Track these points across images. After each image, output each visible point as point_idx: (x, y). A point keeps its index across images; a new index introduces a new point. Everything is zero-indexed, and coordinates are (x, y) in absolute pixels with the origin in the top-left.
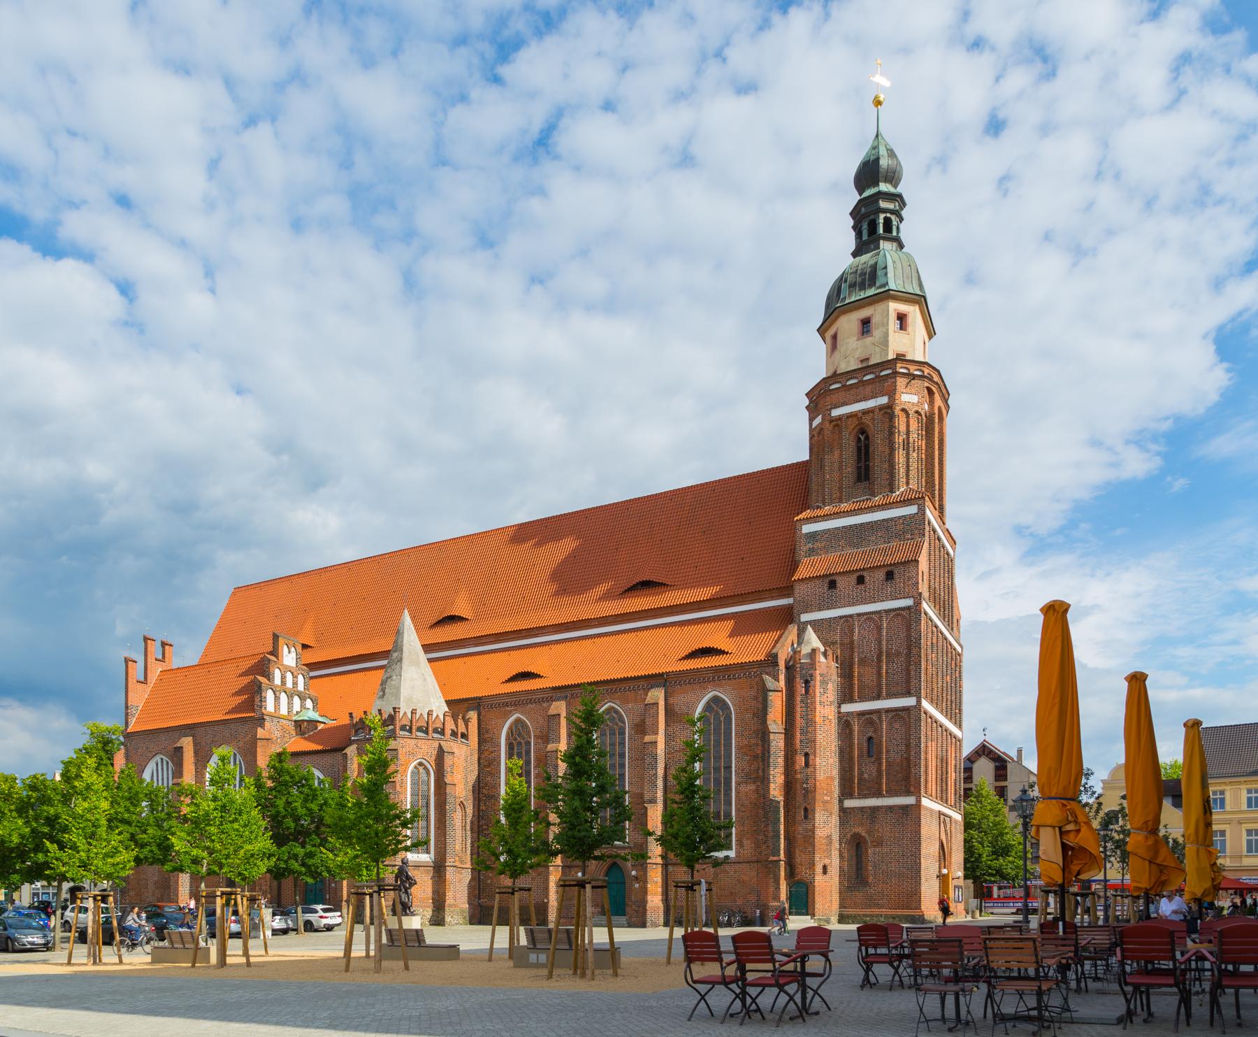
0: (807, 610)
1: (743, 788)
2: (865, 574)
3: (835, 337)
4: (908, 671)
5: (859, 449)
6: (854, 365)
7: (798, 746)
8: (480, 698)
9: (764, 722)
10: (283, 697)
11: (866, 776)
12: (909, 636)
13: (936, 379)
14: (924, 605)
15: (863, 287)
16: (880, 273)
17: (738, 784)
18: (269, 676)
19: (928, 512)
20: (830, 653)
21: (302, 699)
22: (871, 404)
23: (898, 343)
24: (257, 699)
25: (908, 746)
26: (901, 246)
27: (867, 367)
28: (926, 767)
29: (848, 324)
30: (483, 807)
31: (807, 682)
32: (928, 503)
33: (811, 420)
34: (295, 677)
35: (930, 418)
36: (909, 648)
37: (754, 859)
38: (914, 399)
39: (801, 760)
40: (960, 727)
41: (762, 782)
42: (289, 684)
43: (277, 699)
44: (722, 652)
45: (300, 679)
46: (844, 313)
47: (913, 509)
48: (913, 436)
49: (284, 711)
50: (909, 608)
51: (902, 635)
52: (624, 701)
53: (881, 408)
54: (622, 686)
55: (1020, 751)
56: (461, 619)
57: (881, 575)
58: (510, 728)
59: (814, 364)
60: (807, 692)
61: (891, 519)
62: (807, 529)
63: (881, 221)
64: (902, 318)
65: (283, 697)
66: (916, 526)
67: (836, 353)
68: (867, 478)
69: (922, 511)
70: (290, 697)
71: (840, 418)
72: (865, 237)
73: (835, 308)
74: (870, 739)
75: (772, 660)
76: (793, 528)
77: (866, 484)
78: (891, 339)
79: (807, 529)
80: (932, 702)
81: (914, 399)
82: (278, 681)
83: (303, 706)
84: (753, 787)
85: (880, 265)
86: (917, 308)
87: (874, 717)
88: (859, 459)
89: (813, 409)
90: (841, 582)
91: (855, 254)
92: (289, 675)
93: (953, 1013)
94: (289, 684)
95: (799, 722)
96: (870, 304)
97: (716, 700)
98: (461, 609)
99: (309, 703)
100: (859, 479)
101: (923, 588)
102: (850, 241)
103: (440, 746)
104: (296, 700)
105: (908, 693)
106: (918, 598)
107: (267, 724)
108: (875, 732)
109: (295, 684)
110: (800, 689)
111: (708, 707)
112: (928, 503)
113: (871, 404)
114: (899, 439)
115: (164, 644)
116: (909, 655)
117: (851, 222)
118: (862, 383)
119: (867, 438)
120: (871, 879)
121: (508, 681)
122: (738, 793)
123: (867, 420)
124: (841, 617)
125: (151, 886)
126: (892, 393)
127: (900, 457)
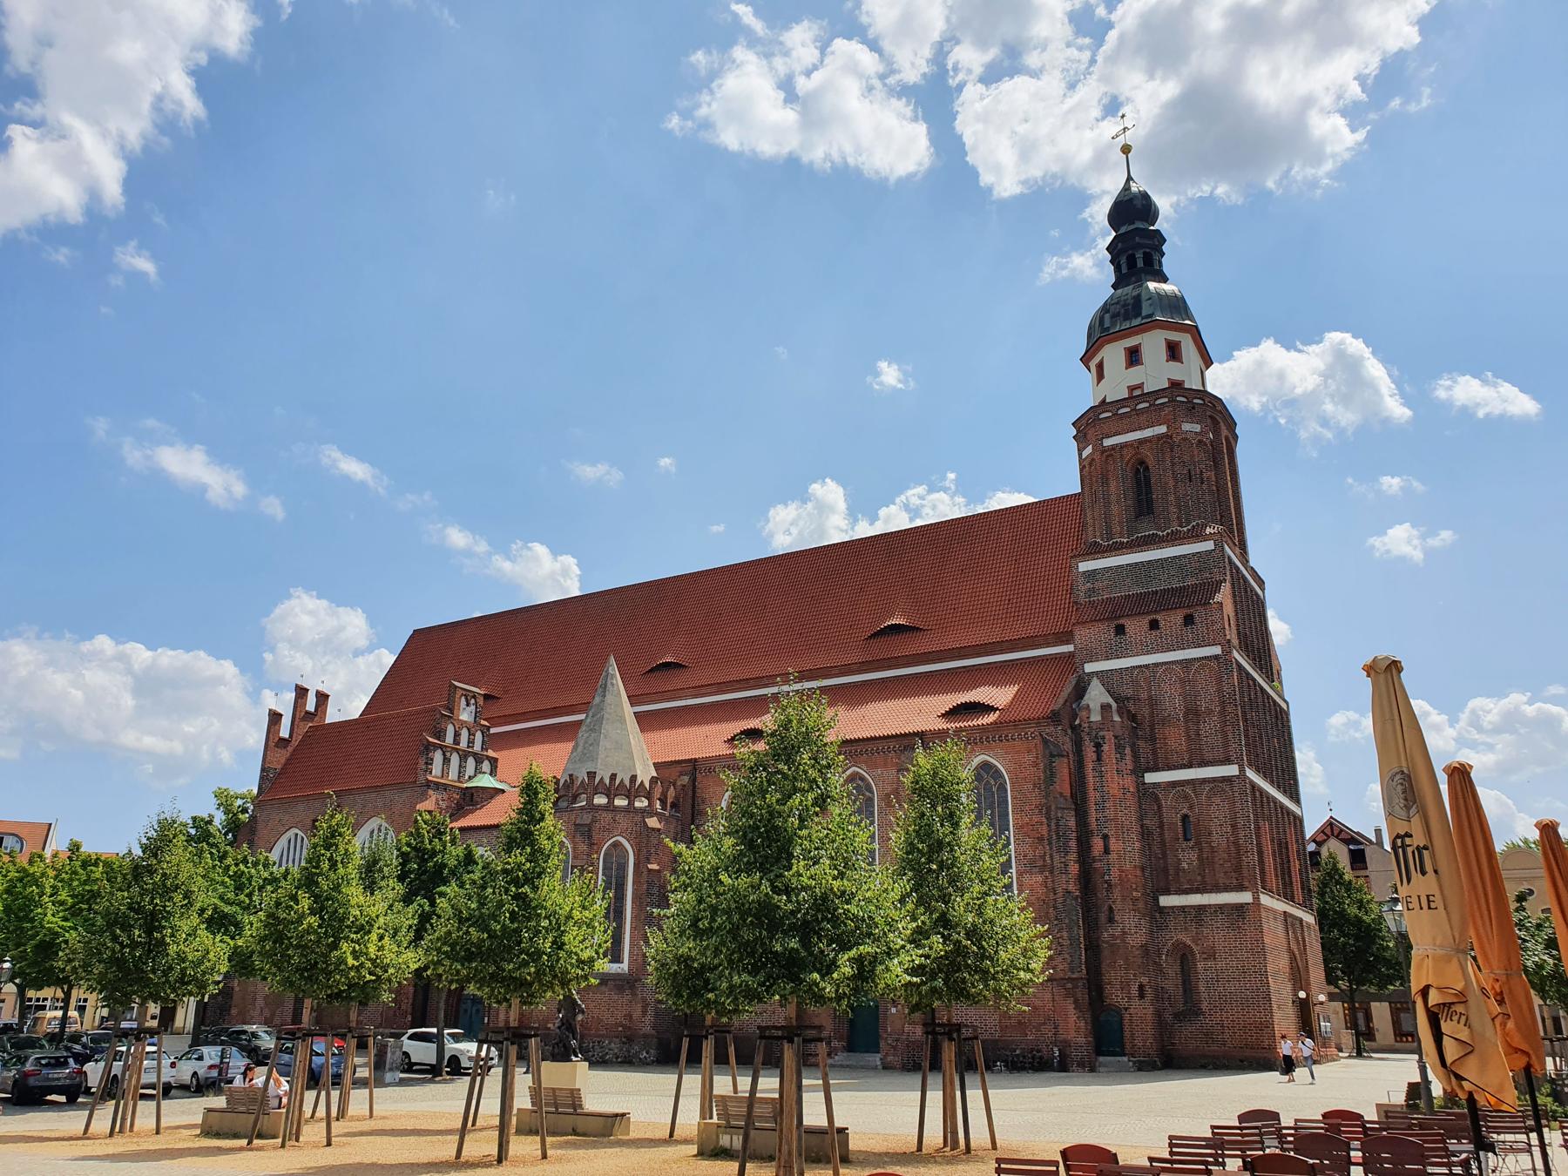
1: (1026, 878)
2: (1158, 617)
3: (1100, 366)
5: (1138, 482)
7: (1094, 826)
10: (455, 759)
15: (1127, 318)
18: (440, 734)
22: (1148, 433)
29: (1113, 355)
31: (1098, 746)
33: (1080, 451)
38: (1197, 428)
39: (1097, 844)
42: (463, 744)
43: (446, 761)
46: (1109, 342)
50: (1216, 657)
52: (872, 766)
53: (1159, 437)
57: (1178, 617)
59: (1083, 394)
60: (1099, 759)
61: (1184, 556)
62: (1084, 566)
68: (1150, 511)
71: (1113, 447)
72: (1124, 270)
73: (1103, 331)
74: (1185, 818)
79: (1084, 566)
80: (1258, 771)
82: (449, 740)
84: (1040, 879)
89: (1081, 438)
91: (1115, 286)
94: (463, 744)
95: (1093, 796)
96: (1137, 333)
97: (985, 766)
99: (486, 766)
102: (1109, 274)
108: (1191, 808)
109: (471, 742)
110: (1089, 753)
113: (1148, 433)
119: (1147, 468)
120: (1204, 1006)
124: (1134, 668)
125: (260, 1002)
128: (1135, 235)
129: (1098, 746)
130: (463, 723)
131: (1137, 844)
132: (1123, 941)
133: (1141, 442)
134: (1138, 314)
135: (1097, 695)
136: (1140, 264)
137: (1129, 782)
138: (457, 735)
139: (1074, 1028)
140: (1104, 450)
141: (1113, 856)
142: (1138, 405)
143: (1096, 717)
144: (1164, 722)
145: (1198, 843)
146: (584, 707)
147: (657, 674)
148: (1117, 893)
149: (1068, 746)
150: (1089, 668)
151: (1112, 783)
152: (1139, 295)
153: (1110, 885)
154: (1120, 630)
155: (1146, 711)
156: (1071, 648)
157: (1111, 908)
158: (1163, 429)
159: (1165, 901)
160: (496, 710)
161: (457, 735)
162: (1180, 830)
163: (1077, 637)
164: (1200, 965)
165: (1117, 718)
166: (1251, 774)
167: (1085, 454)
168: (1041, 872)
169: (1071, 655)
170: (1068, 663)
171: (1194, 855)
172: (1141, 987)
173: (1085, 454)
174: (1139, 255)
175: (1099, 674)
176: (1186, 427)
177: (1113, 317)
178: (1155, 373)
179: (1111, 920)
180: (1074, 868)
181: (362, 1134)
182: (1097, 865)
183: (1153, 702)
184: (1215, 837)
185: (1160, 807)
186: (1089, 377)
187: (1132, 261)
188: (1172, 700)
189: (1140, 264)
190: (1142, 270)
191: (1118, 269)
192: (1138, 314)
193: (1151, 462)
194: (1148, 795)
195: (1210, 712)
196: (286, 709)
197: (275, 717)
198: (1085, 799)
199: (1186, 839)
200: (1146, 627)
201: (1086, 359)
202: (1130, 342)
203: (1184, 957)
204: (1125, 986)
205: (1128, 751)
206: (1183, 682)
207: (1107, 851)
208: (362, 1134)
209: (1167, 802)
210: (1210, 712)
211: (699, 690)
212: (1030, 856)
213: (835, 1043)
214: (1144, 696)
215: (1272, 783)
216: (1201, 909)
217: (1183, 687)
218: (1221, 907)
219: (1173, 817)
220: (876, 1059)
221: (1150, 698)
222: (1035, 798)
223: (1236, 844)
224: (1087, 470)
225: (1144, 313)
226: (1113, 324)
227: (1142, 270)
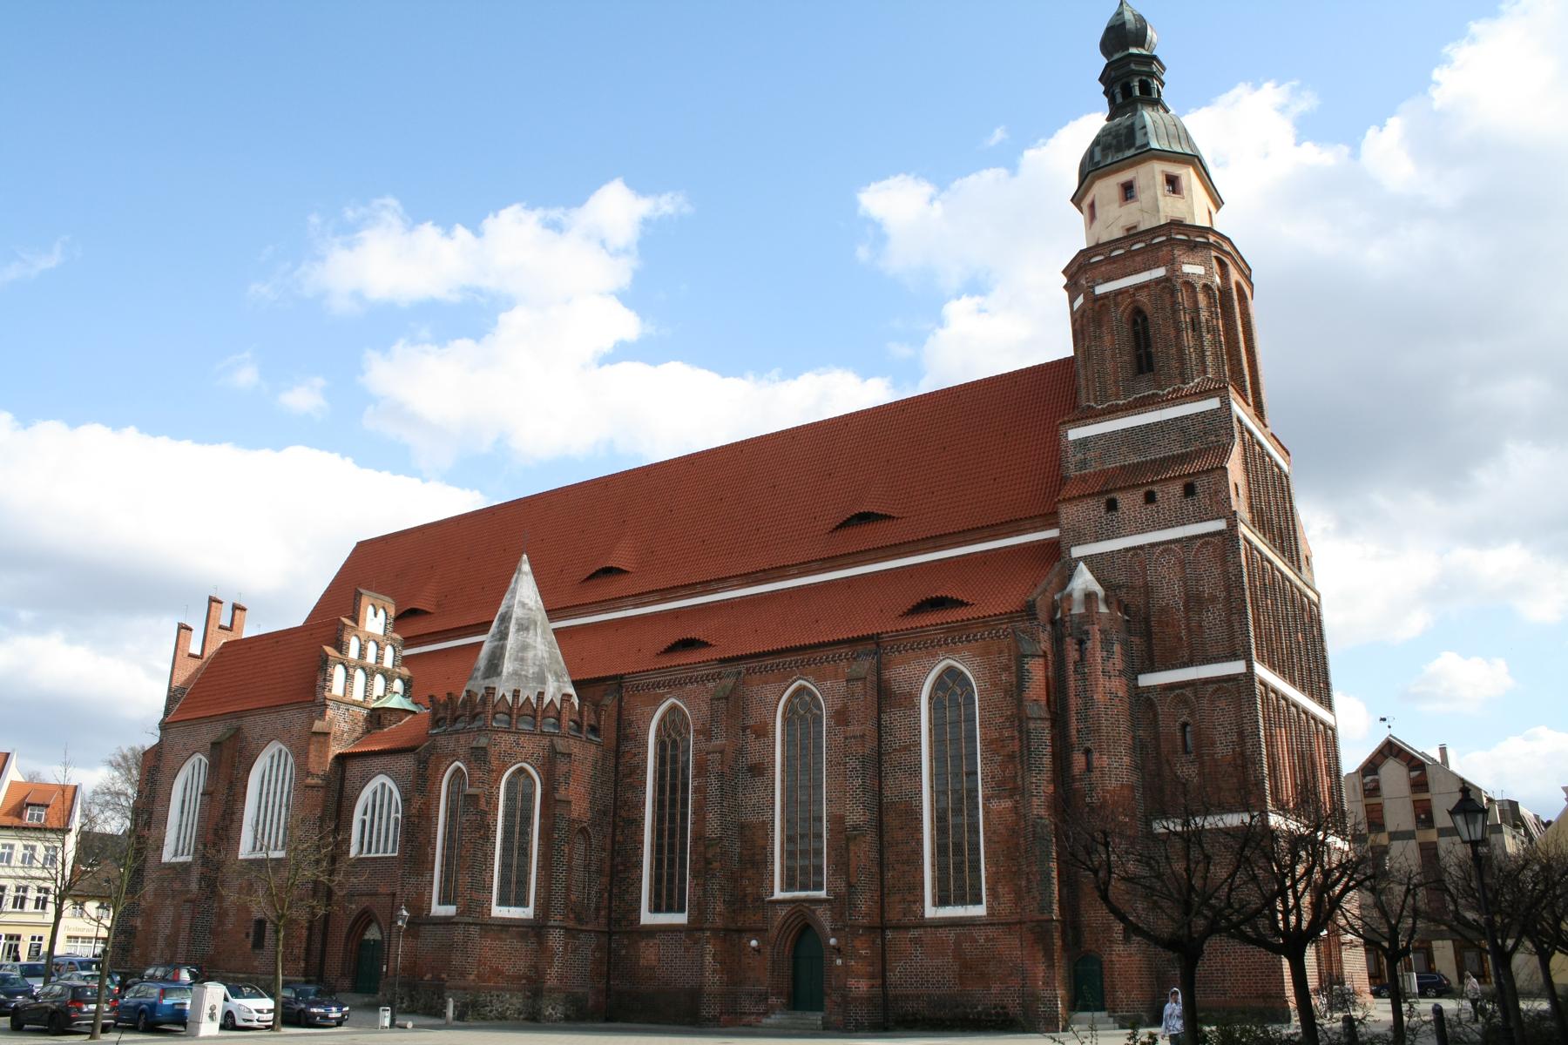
0: (1081, 540)
1: (995, 805)
2: (1155, 488)
3: (1092, 206)
4: (1231, 626)
5: (1136, 334)
6: (1118, 233)
7: (1074, 739)
8: (622, 676)
9: (1020, 702)
12: (1225, 572)
13: (1227, 248)
14: (1243, 530)
15: (1119, 149)
16: (1139, 134)
17: (987, 799)
18: (340, 646)
19: (1235, 407)
20: (1113, 600)
21: (389, 678)
23: (1170, 208)
24: (320, 678)
26: (1167, 111)
27: (1132, 234)
28: (1273, 767)
29: (1108, 188)
30: (619, 838)
31: (1081, 642)
32: (1233, 394)
33: (1072, 302)
35: (1225, 292)
36: (1228, 588)
38: (1200, 270)
39: (1079, 760)
40: (1330, 707)
41: (1022, 795)
42: (371, 658)
43: (349, 677)
44: (961, 604)
45: (389, 652)
46: (1100, 177)
47: (1214, 403)
48: (1204, 315)
49: (358, 695)
50: (1220, 533)
51: (1217, 572)
52: (820, 679)
53: (1158, 281)
54: (819, 655)
55: (1443, 750)
56: (619, 571)
57: (1177, 489)
58: (663, 719)
59: (1073, 236)
61: (1187, 417)
62: (1075, 434)
64: (1173, 182)
65: (359, 676)
66: (1218, 429)
67: (1096, 223)
68: (1150, 368)
69: (1226, 405)
71: (1106, 296)
72: (1119, 99)
73: (1091, 169)
74: (1185, 725)
75: (1029, 611)
76: (1056, 438)
77: (1150, 375)
78: (1161, 204)
79: (1075, 434)
80: (1272, 667)
81: (1200, 270)
82: (353, 653)
84: (1008, 803)
85: (1138, 125)
86: (1191, 170)
87: (1188, 692)
88: (1138, 346)
89: (1072, 287)
90: (1124, 500)
91: (1109, 119)
94: (371, 658)
95: (1074, 703)
96: (1131, 166)
97: (950, 671)
98: (620, 558)
101: (1240, 505)
103: (553, 746)
104: (379, 681)
105: (1233, 657)
106: (1232, 519)
107: (330, 713)
108: (1191, 714)
109: (379, 658)
111: (939, 684)
112: (1233, 394)
114: (1185, 318)
115: (236, 608)
116: (1228, 599)
117: (1102, 88)
118: (1131, 254)
119: (1145, 319)
121: (671, 649)
122: (986, 813)
123: (1143, 297)
124: (1127, 550)
125: (161, 943)
126: (1171, 263)
127: (1188, 339)
129: (1081, 642)
131: (1126, 760)
133: (1139, 288)
134: (1131, 145)
135: (1084, 580)
137: (1117, 685)
141: (1096, 774)
143: (1078, 609)
145: (1199, 756)
147: (594, 582)
151: (1106, 684)
154: (1112, 506)
155: (1140, 601)
156: (1053, 533)
158: (1160, 272)
160: (418, 626)
161: (362, 651)
162: (1179, 742)
163: (1063, 516)
165: (1103, 609)
166: (1261, 671)
168: (1011, 796)
170: (1053, 553)
182: (1077, 785)
183: (1148, 590)
185: (1156, 715)
186: (1078, 218)
187: (1127, 90)
188: (1170, 591)
191: (1112, 101)
192: (1131, 145)
193: (1148, 309)
194: (1144, 702)
195: (1213, 599)
198: (1065, 708)
199: (1186, 752)
201: (1077, 200)
202: (1125, 176)
205: (1117, 648)
206: (1182, 564)
207: (1089, 767)
211: (640, 598)
213: (773, 1000)
215: (1293, 683)
217: (1183, 568)
219: (1169, 724)
220: (816, 1018)
221: (1146, 584)
223: (1242, 754)
224: (1085, 324)
225: (1138, 143)
226: (1105, 156)
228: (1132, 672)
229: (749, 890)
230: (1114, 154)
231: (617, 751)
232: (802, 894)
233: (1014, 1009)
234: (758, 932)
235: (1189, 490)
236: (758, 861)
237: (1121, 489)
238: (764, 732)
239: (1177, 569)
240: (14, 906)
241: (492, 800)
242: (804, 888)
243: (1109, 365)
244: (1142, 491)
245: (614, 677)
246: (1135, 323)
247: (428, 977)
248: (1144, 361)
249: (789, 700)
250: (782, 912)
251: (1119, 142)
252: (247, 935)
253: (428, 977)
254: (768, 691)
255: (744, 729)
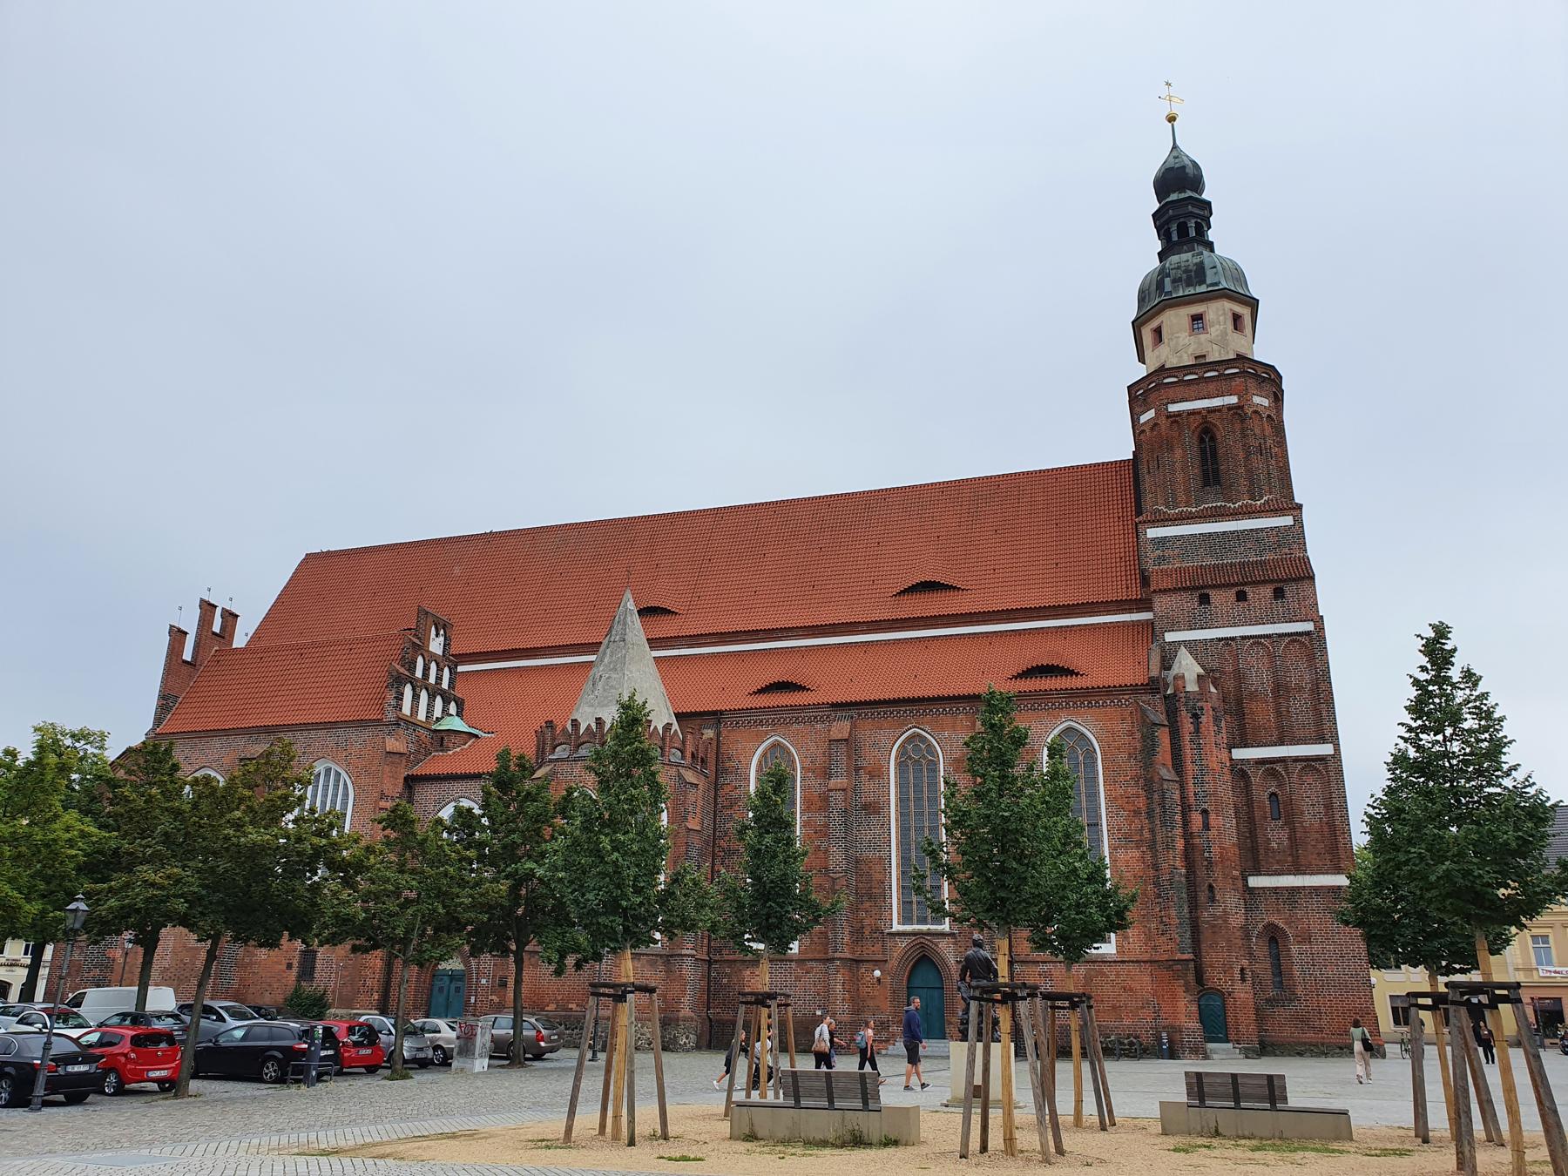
1: (1121, 854)
2: (1247, 589)
5: (1203, 451)
8: (721, 712)
10: (424, 695)
11: (1274, 845)
25: (1329, 807)
27: (1201, 364)
29: (1175, 320)
31: (1196, 716)
34: (440, 670)
37: (1146, 957)
39: (1197, 819)
42: (432, 680)
43: (416, 697)
46: (1171, 306)
49: (422, 716)
50: (1308, 633)
53: (1230, 408)
57: (1267, 591)
60: (1197, 730)
61: (1262, 530)
62: (1153, 533)
63: (1174, 227)
65: (424, 695)
68: (1217, 481)
70: (432, 698)
71: (1179, 414)
72: (1175, 237)
79: (1153, 533)
83: (445, 711)
87: (1278, 768)
88: (1204, 461)
90: (1216, 597)
91: (1162, 256)
92: (433, 666)
93: (992, 1113)
94: (432, 680)
96: (1202, 301)
97: (775, 745)
99: (453, 708)
100: (1206, 483)
105: (1321, 739)
108: (1279, 786)
109: (439, 679)
110: (1187, 725)
118: (1202, 379)
119: (1213, 439)
120: (1299, 991)
121: (762, 691)
123: (1212, 418)
124: (1220, 640)
128: (1181, 204)
129: (1196, 716)
130: (433, 655)
132: (1225, 921)
133: (1211, 411)
134: (1202, 282)
136: (1193, 233)
138: (426, 669)
139: (1185, 1013)
140: (1170, 416)
141: (1213, 832)
142: (1204, 375)
144: (1253, 696)
146: (593, 647)
148: (1218, 872)
149: (1162, 718)
150: (1170, 637)
152: (1202, 262)
153: (1210, 863)
154: (1205, 600)
157: (1211, 887)
158: (1233, 400)
159: (1254, 882)
161: (426, 669)
164: (1294, 949)
167: (1144, 419)
168: (1138, 847)
169: (1150, 624)
170: (1150, 631)
171: (1284, 836)
172: (1242, 970)
173: (1144, 419)
174: (1192, 224)
175: (1191, 645)
176: (1257, 400)
177: (1174, 281)
178: (1218, 341)
179: (1213, 899)
180: (1180, 844)
181: (453, 1136)
182: (1197, 841)
184: (1307, 817)
187: (1183, 230)
188: (1259, 676)
189: (1193, 233)
190: (1193, 240)
194: (1240, 772)
195: (1300, 689)
196: (191, 626)
197: (177, 635)
200: (1233, 598)
203: (1274, 936)
204: (1227, 969)
207: (1206, 826)
208: (453, 1136)
209: (1256, 779)
210: (1300, 689)
212: (1125, 829)
214: (1229, 669)
216: (1294, 890)
218: (1316, 889)
222: (1131, 768)
226: (1176, 289)
227: (1193, 240)
228: (1230, 748)
229: (866, 922)
230: (1156, 300)
231: (716, 784)
232: (924, 928)
233: (1147, 1039)
234: (878, 963)
235: (1279, 594)
236: (873, 894)
237: (1214, 587)
238: (878, 773)
239: (1266, 660)
240: (1397, 1022)
241: (884, 862)
242: (923, 921)
243: (1180, 477)
244: (1234, 590)
245: (714, 713)
246: (1202, 440)
247: (552, 1007)
248: (1211, 474)
249: (902, 746)
250: (903, 944)
251: (1189, 277)
252: (289, 966)
253: (552, 1007)
254: (883, 736)
255: (857, 769)
